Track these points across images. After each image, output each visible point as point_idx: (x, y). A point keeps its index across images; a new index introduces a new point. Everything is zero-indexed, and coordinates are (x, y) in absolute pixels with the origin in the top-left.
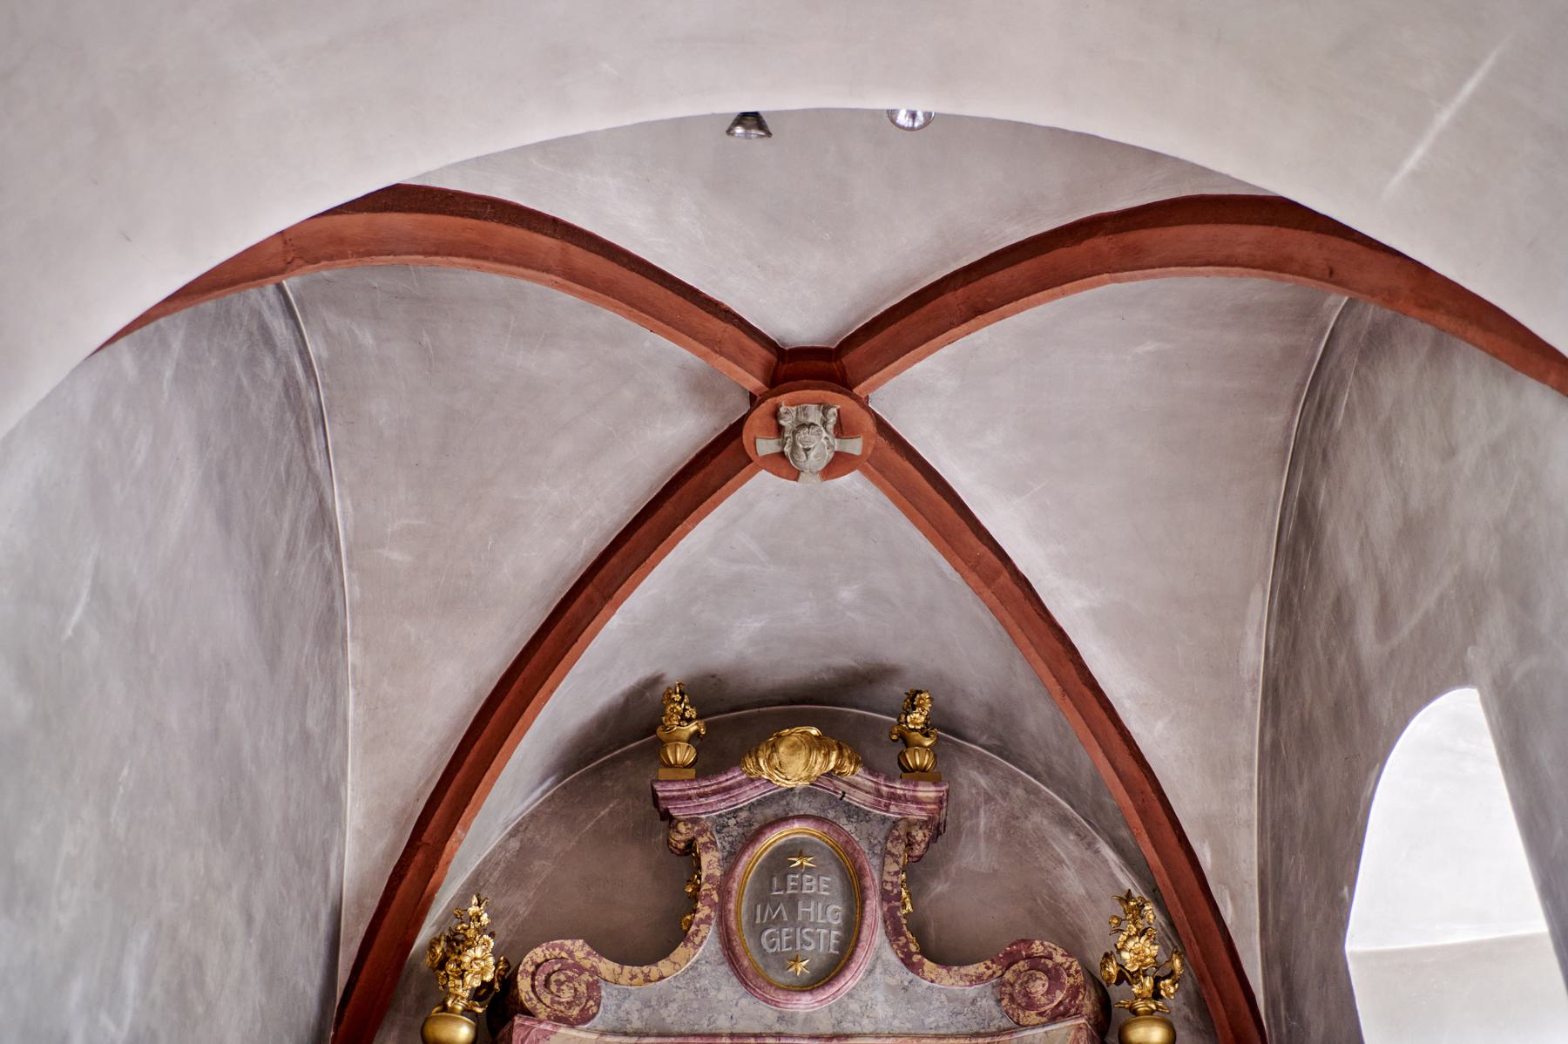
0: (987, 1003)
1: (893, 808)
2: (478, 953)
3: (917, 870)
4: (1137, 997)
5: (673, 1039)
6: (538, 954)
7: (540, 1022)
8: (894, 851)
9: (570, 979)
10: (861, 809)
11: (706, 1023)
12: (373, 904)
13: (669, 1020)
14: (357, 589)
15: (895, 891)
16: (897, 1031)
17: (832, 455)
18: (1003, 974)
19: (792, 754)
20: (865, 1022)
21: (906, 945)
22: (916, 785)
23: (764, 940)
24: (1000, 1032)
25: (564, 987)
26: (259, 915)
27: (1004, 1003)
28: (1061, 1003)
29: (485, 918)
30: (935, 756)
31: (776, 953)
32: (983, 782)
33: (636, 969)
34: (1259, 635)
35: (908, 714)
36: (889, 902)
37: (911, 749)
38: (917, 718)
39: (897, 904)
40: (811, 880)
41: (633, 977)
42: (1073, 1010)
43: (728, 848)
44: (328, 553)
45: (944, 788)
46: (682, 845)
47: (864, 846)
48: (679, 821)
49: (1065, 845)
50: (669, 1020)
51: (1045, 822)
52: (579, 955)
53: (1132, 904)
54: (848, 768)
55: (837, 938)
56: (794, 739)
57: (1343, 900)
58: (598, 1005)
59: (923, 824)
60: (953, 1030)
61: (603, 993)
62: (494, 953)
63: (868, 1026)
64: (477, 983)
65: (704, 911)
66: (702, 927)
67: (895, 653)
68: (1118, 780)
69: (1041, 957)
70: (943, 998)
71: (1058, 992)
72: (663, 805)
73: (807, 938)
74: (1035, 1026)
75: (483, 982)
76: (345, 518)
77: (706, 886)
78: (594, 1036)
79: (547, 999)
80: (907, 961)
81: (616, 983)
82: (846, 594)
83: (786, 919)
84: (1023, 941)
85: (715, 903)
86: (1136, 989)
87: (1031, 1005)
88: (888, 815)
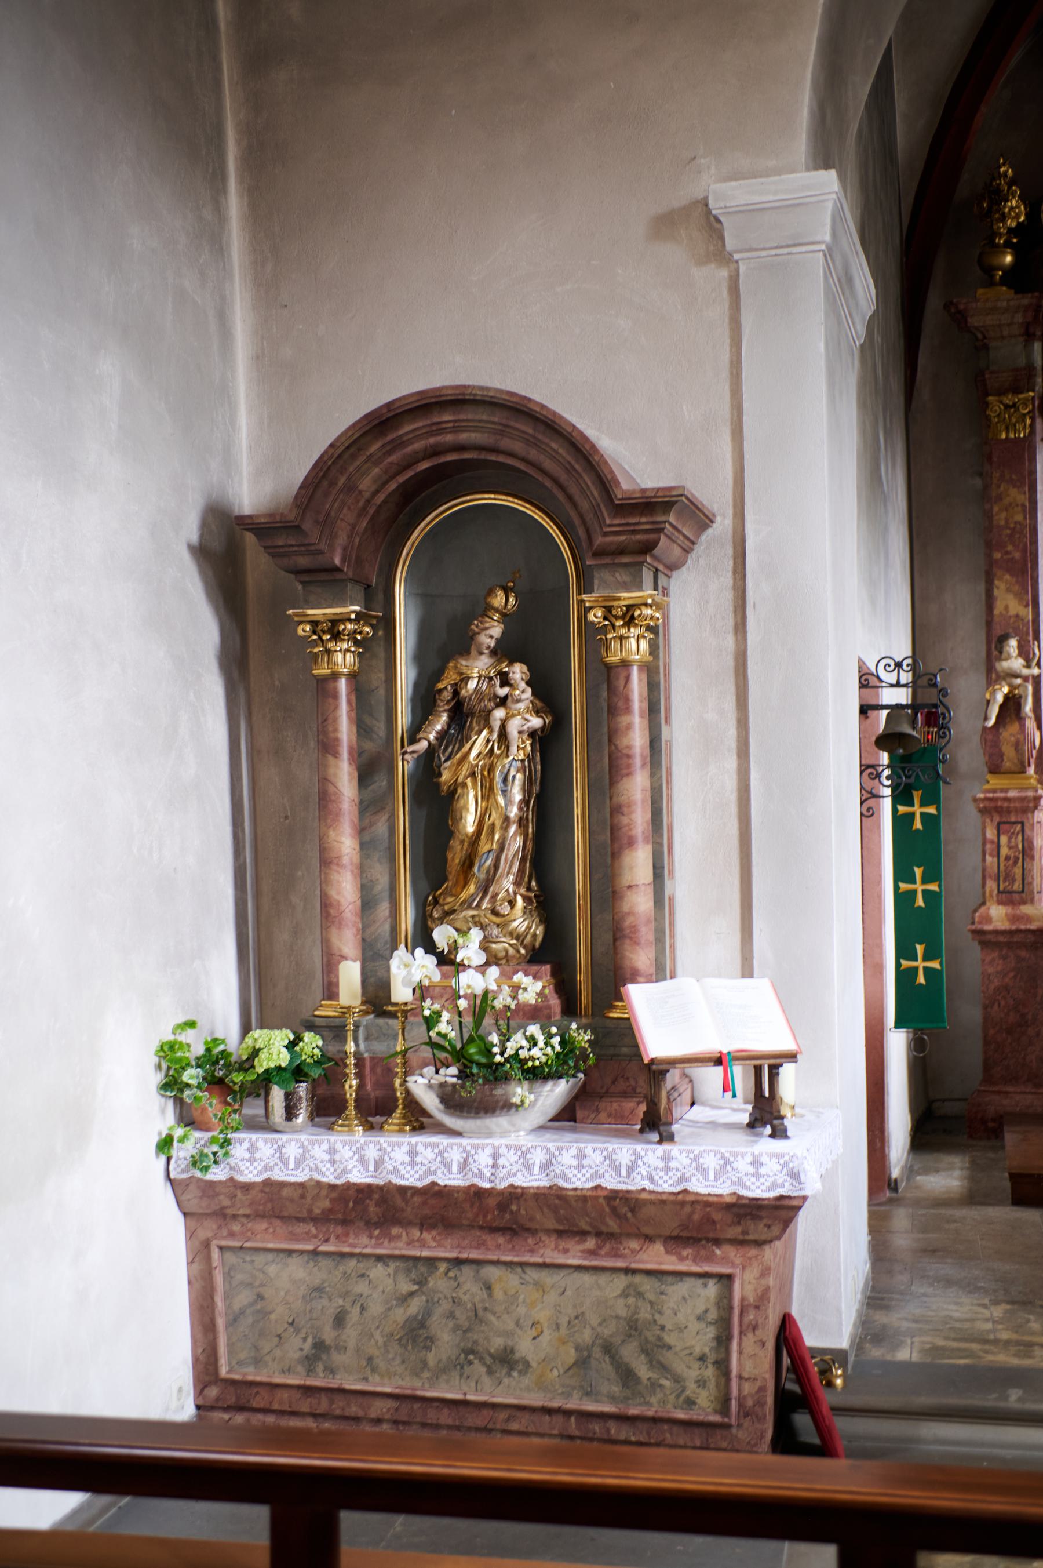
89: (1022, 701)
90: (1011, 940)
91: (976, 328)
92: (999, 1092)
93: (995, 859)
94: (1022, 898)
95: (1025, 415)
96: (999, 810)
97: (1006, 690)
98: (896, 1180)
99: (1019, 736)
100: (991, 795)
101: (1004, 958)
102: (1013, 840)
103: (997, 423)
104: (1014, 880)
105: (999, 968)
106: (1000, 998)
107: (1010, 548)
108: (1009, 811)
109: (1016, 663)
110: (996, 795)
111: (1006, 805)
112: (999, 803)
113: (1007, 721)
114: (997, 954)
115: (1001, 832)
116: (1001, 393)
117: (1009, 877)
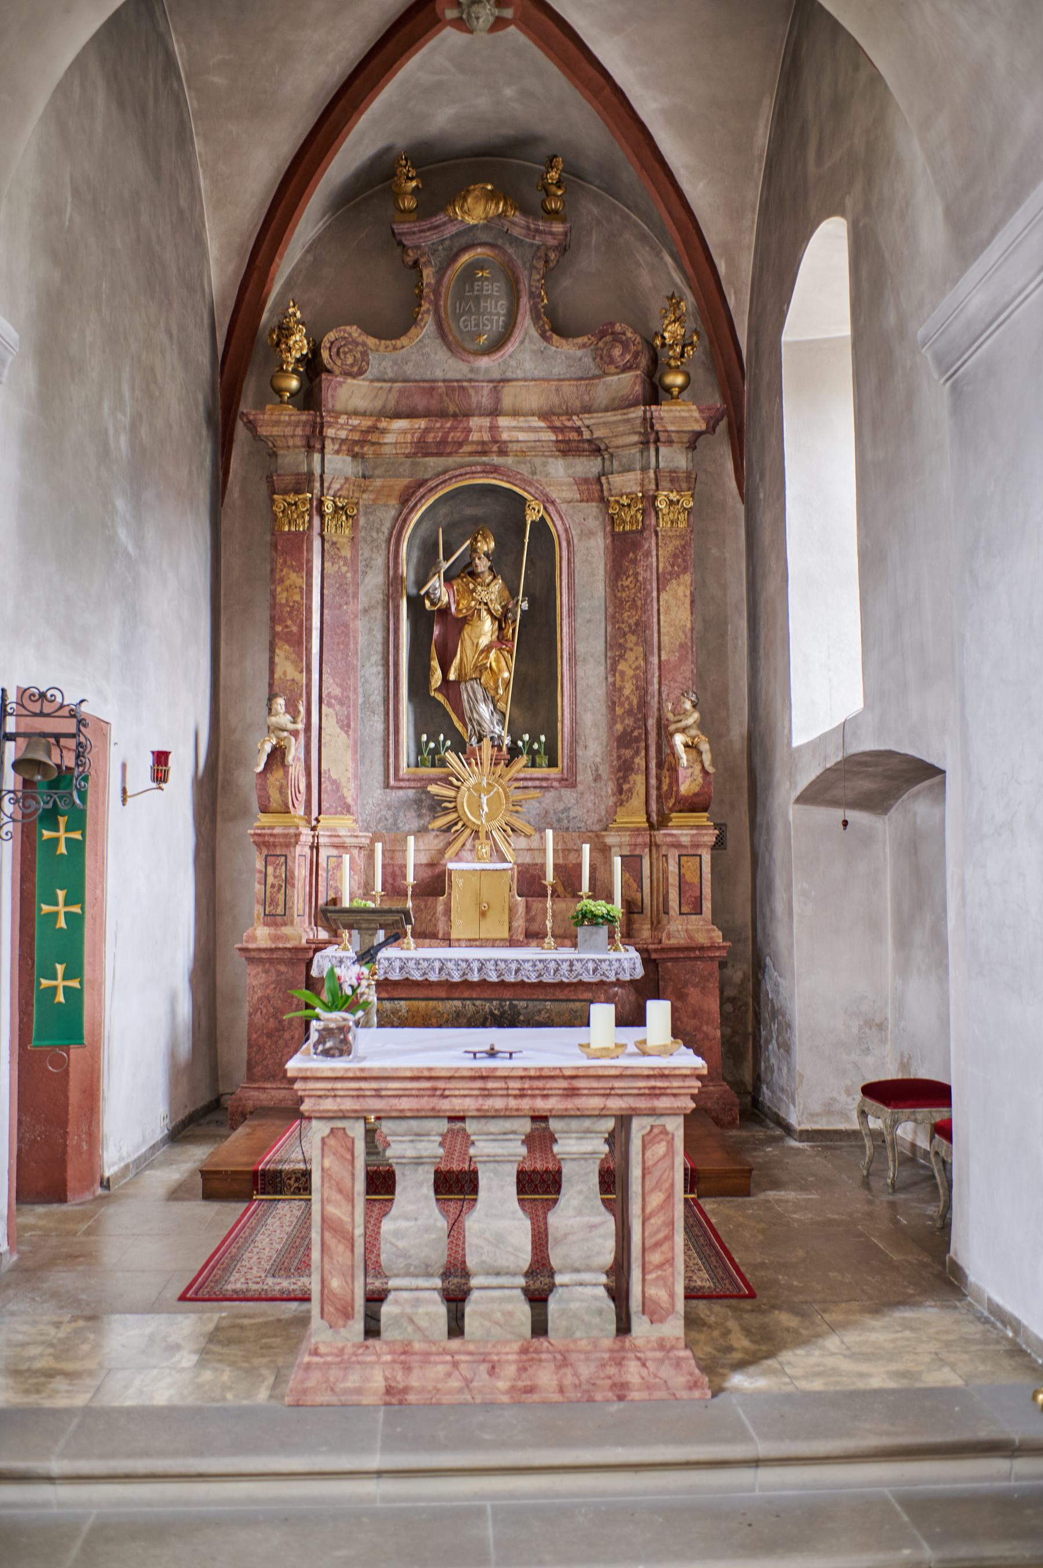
0: (588, 360)
2: (298, 337)
3: (550, 275)
4: (671, 358)
6: (331, 336)
9: (351, 351)
12: (231, 304)
14: (195, 103)
20: (519, 372)
21: (543, 325)
23: (461, 323)
24: (594, 377)
26: (175, 331)
29: (298, 314)
32: (595, 211)
33: (388, 342)
34: (766, 126)
38: (553, 175)
41: (387, 347)
44: (175, 85)
46: (411, 263)
49: (643, 255)
51: (632, 239)
52: (355, 335)
54: (510, 213)
56: (477, 192)
59: (555, 248)
60: (568, 376)
62: (307, 336)
63: (520, 374)
64: (298, 356)
65: (426, 306)
66: (425, 316)
67: (541, 128)
72: (398, 237)
77: (426, 290)
78: (367, 383)
79: (339, 363)
80: (543, 336)
82: (509, 92)
86: (671, 353)
87: (612, 361)
91: (266, 437)
92: (258, 1088)
96: (266, 844)
98: (108, 1179)
100: (259, 831)
101: (267, 972)
104: (277, 905)
105: (262, 981)
107: (289, 623)
109: (283, 719)
110: (263, 831)
111: (272, 840)
112: (267, 839)
116: (285, 492)
117: (274, 902)
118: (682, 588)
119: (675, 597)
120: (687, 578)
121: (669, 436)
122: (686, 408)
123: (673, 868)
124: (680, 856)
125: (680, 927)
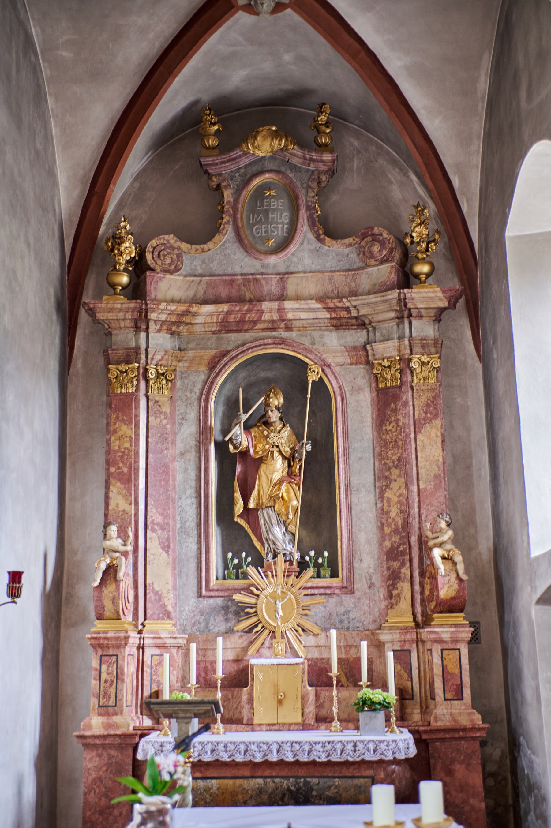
0: (354, 256)
1: (312, 165)
2: (127, 244)
4: (418, 252)
5: (216, 278)
6: (154, 243)
7: (158, 273)
8: (312, 186)
9: (169, 253)
10: (297, 166)
11: (230, 269)
12: (76, 220)
13: (214, 269)
15: (313, 205)
16: (314, 270)
17: (274, 5)
18: (360, 243)
19: (264, 140)
20: (300, 266)
21: (318, 231)
22: (322, 154)
23: (254, 231)
24: (359, 269)
25: (167, 257)
26: (32, 240)
27: (360, 256)
28: (385, 256)
29: (128, 227)
30: (332, 138)
31: (260, 236)
32: (356, 143)
33: (198, 247)
35: (319, 116)
36: (310, 211)
37: (320, 135)
39: (314, 211)
40: (274, 202)
41: (197, 250)
42: (390, 259)
43: (236, 187)
44: (33, 58)
45: (335, 155)
46: (214, 187)
47: (298, 184)
48: (213, 175)
49: (394, 174)
50: (214, 269)
51: (385, 163)
52: (172, 241)
53: (419, 209)
54: (290, 147)
55: (287, 228)
56: (264, 133)
57: (506, 214)
58: (182, 264)
59: (326, 172)
60: (338, 268)
61: (184, 258)
63: (301, 268)
64: (128, 258)
65: (226, 218)
66: (226, 226)
67: (313, 83)
68: (416, 150)
69: (377, 235)
70: (334, 254)
71: (384, 251)
72: (205, 168)
73: (273, 229)
74: (373, 266)
75: (131, 257)
76: (37, 35)
77: (226, 207)
78: (182, 278)
79: (160, 263)
80: (318, 238)
81: (189, 253)
82: (287, 57)
83: (263, 221)
84: (370, 227)
85: (231, 215)
87: (372, 256)
88: (309, 168)
89: (118, 568)
90: (104, 742)
91: (103, 320)
93: (98, 682)
94: (115, 710)
95: (132, 378)
96: (101, 646)
97: (108, 561)
99: (115, 593)
100: (95, 636)
101: (100, 756)
102: (110, 668)
103: (115, 382)
104: (110, 697)
105: (96, 764)
106: (95, 787)
107: (121, 465)
108: (108, 647)
110: (99, 635)
111: (105, 642)
112: (101, 641)
113: (108, 582)
114: (95, 752)
115: (102, 662)
116: (118, 363)
117: (106, 695)
118: (434, 430)
119: (429, 437)
120: (438, 422)
121: (420, 312)
122: (432, 290)
123: (437, 660)
124: (442, 650)
125: (445, 711)
